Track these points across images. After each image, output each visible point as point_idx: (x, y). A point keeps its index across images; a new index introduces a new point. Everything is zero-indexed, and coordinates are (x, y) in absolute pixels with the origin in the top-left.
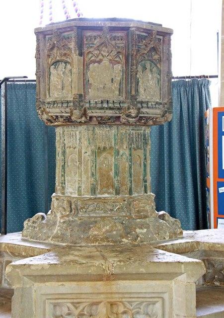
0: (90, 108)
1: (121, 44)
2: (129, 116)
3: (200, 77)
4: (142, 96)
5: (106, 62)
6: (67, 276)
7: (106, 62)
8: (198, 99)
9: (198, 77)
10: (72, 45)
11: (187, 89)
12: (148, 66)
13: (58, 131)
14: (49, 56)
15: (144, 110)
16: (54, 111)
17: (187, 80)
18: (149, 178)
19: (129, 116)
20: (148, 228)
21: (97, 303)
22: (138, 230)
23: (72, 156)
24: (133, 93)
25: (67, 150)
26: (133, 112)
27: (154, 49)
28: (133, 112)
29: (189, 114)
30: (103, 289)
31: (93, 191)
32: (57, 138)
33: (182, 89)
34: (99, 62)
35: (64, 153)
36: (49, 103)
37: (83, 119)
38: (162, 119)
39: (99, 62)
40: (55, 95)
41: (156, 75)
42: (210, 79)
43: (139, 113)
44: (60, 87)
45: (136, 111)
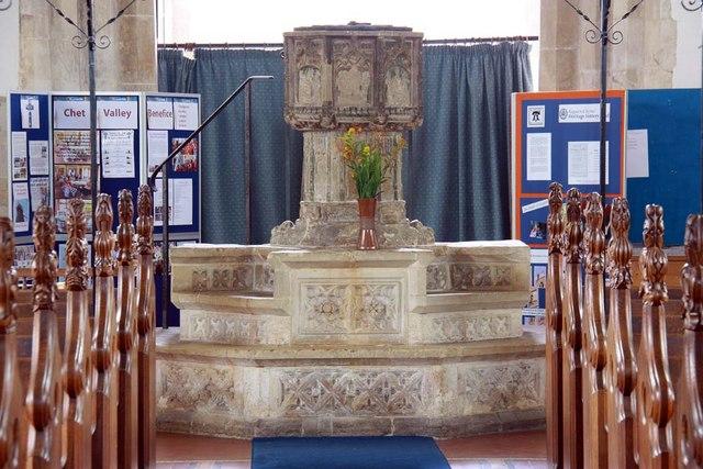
0: (339, 115)
1: (369, 51)
2: (377, 122)
3: (515, 39)
4: (391, 102)
5: (354, 69)
6: (317, 263)
7: (354, 69)
8: (510, 74)
9: (510, 39)
10: (321, 53)
11: (495, 58)
12: (397, 72)
13: (306, 136)
14: (298, 61)
15: (392, 116)
16: (303, 117)
17: (495, 43)
18: (400, 184)
19: (377, 122)
20: (396, 233)
21: (343, 287)
22: (385, 234)
23: (321, 163)
24: (381, 100)
25: (317, 156)
26: (381, 119)
27: (404, 55)
28: (381, 119)
29: (496, 98)
30: (348, 275)
31: (342, 196)
32: (306, 144)
33: (486, 59)
34: (348, 69)
35: (313, 159)
36: (298, 108)
37: (332, 126)
38: (412, 125)
39: (348, 69)
40: (304, 100)
41: (405, 80)
42: (530, 42)
43: (387, 119)
44: (308, 93)
45: (384, 118)
